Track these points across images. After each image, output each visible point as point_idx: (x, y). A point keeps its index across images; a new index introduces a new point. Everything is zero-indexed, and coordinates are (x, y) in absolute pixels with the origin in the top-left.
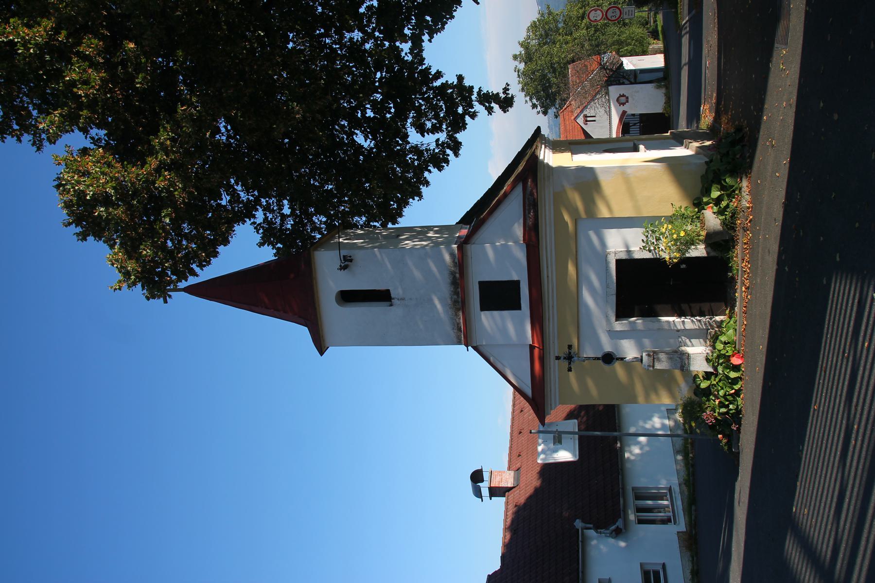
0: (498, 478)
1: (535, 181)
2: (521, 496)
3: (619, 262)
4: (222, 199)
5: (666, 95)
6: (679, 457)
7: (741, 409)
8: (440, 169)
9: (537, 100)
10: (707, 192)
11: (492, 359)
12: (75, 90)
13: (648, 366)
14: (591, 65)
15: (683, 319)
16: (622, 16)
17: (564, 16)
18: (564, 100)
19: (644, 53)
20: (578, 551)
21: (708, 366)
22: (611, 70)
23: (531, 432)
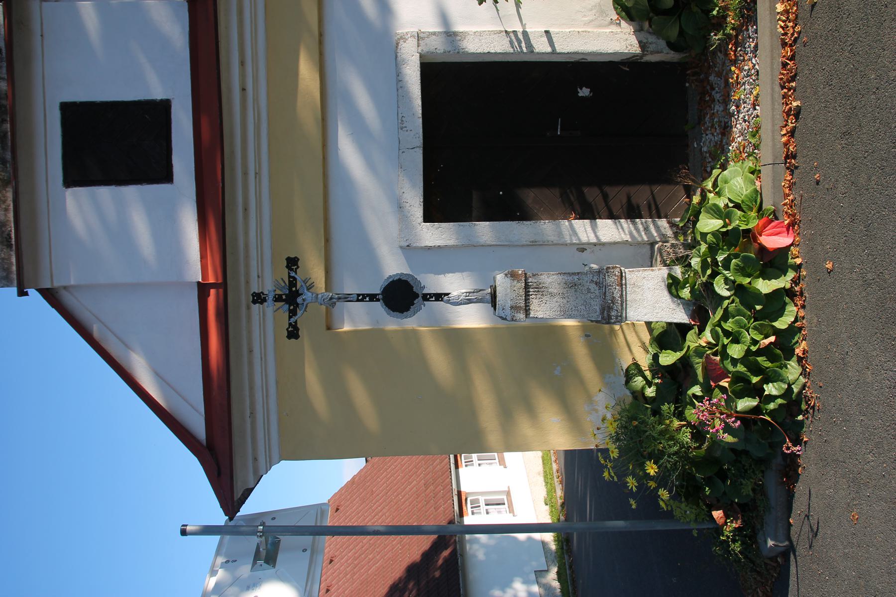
7: (800, 393)
13: (512, 307)
21: (673, 306)
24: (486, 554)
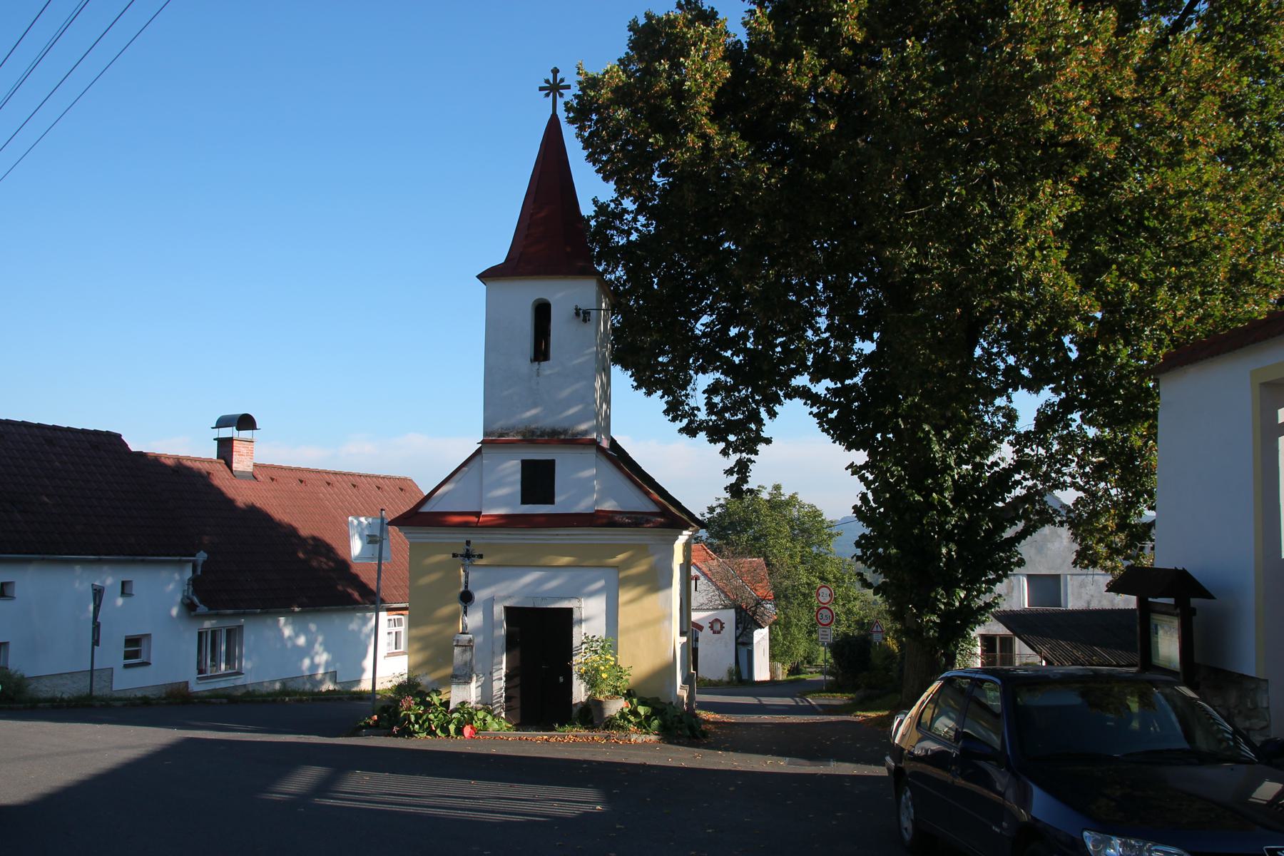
0: (244, 451)
1: (662, 526)
2: (221, 479)
3: (569, 611)
4: (659, 176)
5: (720, 681)
6: (277, 686)
8: (666, 412)
9: (719, 514)
10: (643, 702)
11: (465, 469)
12: (793, 61)
14: (762, 587)
15: (504, 679)
17: (826, 554)
18: (717, 550)
19: (773, 657)
20: (168, 555)
22: (755, 613)
23: (382, 510)
24: (353, 631)
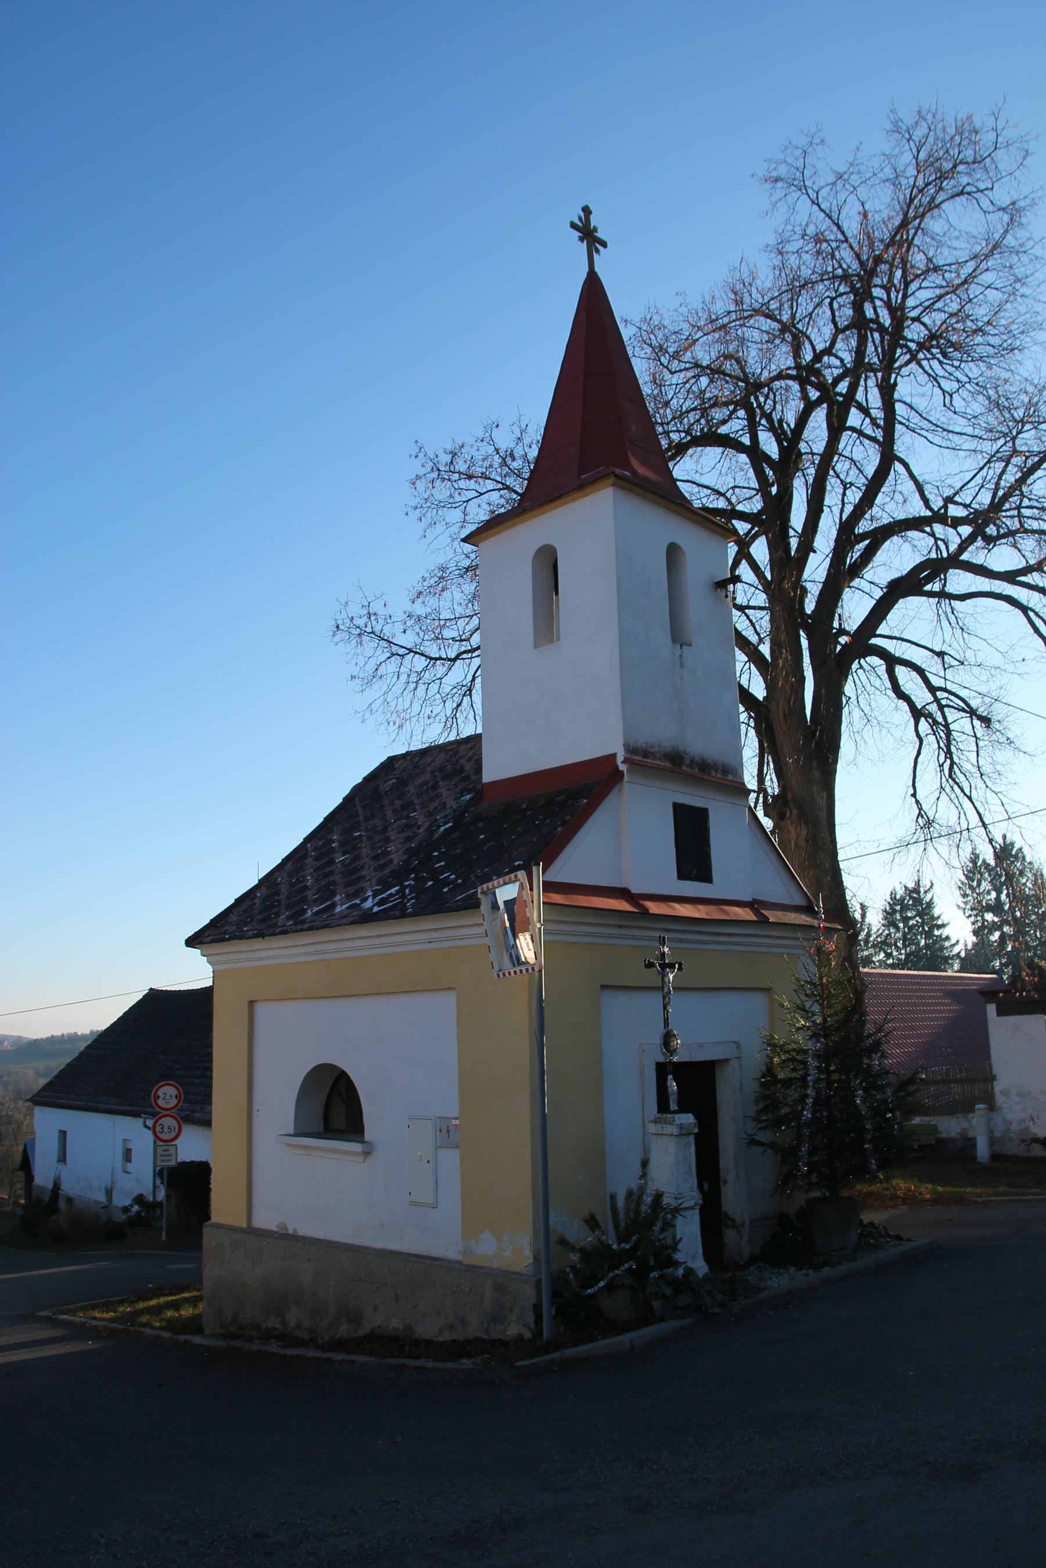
16: (161, 1144)
